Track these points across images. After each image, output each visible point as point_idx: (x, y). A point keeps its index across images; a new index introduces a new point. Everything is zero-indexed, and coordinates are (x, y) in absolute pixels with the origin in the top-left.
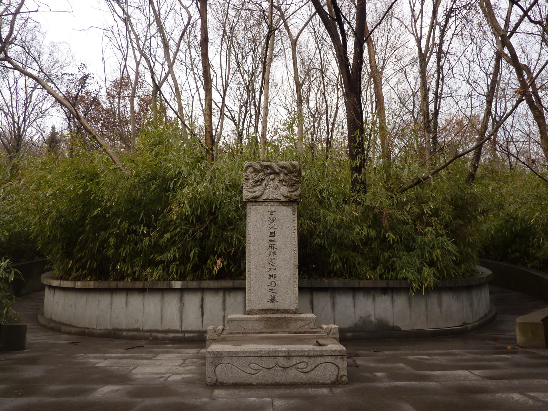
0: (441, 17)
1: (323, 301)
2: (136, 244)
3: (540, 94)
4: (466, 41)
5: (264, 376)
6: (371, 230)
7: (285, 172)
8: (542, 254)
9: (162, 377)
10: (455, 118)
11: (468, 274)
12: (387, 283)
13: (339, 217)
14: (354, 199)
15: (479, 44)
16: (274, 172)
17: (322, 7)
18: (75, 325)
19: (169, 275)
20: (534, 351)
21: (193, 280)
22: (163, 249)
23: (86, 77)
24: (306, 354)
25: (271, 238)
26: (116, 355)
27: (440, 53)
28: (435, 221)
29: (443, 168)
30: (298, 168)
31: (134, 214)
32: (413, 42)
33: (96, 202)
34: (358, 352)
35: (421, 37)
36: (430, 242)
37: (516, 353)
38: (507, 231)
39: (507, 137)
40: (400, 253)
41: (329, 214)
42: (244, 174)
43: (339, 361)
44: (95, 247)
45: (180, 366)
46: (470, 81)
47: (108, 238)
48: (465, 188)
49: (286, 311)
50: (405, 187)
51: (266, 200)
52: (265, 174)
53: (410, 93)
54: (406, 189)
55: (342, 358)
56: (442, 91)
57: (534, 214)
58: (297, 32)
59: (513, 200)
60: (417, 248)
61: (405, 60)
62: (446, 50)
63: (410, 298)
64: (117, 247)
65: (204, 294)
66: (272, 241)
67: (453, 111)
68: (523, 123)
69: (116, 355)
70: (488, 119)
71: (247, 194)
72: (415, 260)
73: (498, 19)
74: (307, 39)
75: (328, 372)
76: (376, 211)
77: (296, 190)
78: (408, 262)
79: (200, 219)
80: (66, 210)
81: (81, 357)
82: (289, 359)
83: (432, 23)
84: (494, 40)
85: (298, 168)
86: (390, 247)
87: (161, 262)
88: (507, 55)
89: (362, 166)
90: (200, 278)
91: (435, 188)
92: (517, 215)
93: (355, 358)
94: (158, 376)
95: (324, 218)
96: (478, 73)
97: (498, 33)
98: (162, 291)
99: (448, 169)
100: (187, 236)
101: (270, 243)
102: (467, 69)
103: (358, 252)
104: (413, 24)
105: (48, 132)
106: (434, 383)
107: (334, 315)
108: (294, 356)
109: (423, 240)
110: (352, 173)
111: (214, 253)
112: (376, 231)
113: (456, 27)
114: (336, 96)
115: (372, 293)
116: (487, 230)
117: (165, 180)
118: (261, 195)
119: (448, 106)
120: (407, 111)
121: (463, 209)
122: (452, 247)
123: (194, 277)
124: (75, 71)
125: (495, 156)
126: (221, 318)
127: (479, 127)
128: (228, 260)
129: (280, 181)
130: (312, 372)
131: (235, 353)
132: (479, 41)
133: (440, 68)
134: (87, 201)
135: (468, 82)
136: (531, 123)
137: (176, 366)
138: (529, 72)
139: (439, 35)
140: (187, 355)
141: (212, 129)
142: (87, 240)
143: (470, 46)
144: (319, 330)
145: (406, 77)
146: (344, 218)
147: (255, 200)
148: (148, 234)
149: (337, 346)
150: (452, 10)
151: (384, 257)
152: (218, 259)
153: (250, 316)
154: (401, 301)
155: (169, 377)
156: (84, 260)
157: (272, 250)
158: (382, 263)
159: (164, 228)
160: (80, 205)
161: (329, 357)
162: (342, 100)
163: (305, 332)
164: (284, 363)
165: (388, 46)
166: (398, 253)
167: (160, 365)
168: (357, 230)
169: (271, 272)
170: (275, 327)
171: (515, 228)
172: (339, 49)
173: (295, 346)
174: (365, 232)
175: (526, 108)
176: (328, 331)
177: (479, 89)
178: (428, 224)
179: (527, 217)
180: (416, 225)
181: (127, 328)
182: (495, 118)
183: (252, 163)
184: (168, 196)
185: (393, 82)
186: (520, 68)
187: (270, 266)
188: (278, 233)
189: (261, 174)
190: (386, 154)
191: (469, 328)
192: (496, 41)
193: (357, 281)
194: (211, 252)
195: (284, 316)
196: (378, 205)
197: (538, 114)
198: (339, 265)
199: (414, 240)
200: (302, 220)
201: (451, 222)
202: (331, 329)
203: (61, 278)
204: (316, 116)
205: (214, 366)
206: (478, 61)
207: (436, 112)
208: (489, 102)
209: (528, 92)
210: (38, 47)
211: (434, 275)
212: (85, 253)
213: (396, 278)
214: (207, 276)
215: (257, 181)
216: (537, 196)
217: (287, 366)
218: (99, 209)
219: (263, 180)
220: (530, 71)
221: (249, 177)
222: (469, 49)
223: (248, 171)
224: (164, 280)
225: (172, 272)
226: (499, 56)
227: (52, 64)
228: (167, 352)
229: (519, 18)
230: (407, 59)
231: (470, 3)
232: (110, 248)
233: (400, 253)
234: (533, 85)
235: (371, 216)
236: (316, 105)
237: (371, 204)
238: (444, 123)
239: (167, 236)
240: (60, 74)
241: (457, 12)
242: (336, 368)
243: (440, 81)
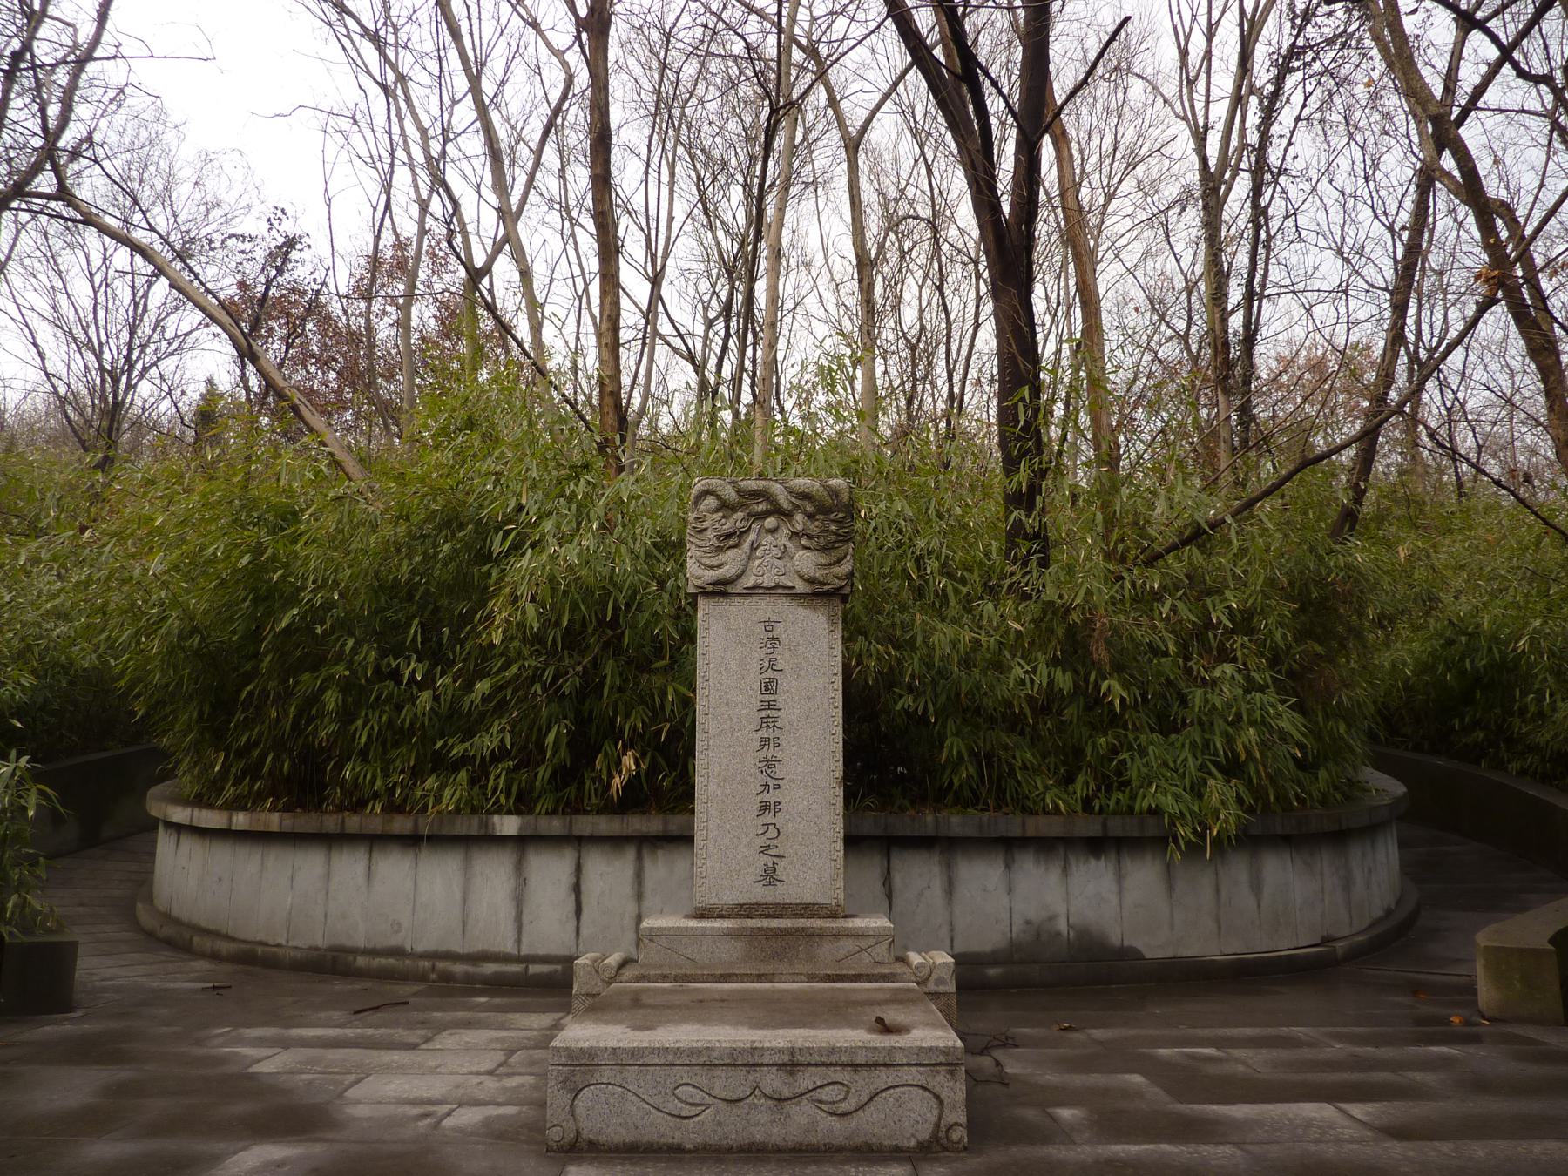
0: (1262, 73)
1: (919, 876)
2: (399, 708)
3: (1546, 286)
4: (1334, 141)
5: (719, 1124)
6: (1059, 671)
7: (809, 508)
8: (1548, 736)
9: (425, 1116)
10: (1304, 353)
11: (1338, 796)
12: (1104, 825)
13: (967, 636)
14: (1010, 586)
15: (1371, 148)
16: (777, 511)
17: (929, 50)
18: (231, 933)
19: (485, 794)
20: (1530, 1032)
21: (552, 812)
22: (471, 726)
23: (291, 243)
24: (844, 1059)
25: (767, 698)
26: (319, 1032)
27: (1262, 174)
28: (1243, 645)
29: (1267, 493)
30: (845, 497)
31: (388, 627)
32: (1184, 143)
33: (288, 590)
34: (1014, 1030)
35: (1206, 128)
36: (1229, 706)
37: (1475, 1039)
38: (1449, 669)
39: (1449, 404)
40: (1143, 738)
41: (940, 626)
42: (691, 517)
43: (940, 1081)
44: (287, 715)
45: (491, 1073)
46: (1346, 250)
47: (322, 690)
48: (1330, 552)
49: (808, 910)
50: (1158, 548)
51: (753, 591)
53: (1180, 284)
54: (1160, 556)
55: (951, 1073)
56: (1265, 276)
57: (1527, 624)
58: (864, 114)
59: (1467, 581)
60: (1192, 723)
61: (1166, 193)
62: (1278, 164)
63: (1168, 868)
64: (346, 716)
66: (769, 706)
67: (1299, 332)
68: (1494, 366)
69: (319, 1032)
70: (1396, 356)
71: (697, 569)
72: (1186, 759)
73: (1426, 72)
74: (894, 136)
75: (909, 1114)
76: (1075, 617)
77: (838, 561)
78: (1165, 764)
79: (574, 639)
80: (205, 613)
81: (221, 1040)
82: (792, 1073)
83: (1238, 88)
84: (1415, 139)
85: (845, 497)
86: (1115, 720)
87: (464, 760)
88: (1448, 174)
89: (1034, 489)
90: (574, 808)
91: (1243, 551)
92: (1478, 626)
93: (999, 1054)
94: (416, 1111)
96: (1369, 228)
97: (1424, 110)
98: (468, 842)
99: (1283, 497)
100: (538, 688)
101: (764, 714)
102: (1337, 218)
103: (1022, 733)
104: (1185, 90)
105: (195, 392)
106: (1228, 1150)
108: (809, 1065)
109: (1207, 701)
110: (1007, 508)
111: (615, 735)
112: (1076, 672)
113: (1306, 98)
114: (973, 294)
115: (1062, 852)
116: (1393, 665)
117: (484, 530)
118: (739, 576)
119: (1286, 320)
120: (1169, 332)
121: (1323, 612)
122: (1289, 722)
123: (557, 802)
124: (251, 225)
125: (1416, 458)
127: (1370, 376)
128: (653, 757)
129: (795, 535)
130: (860, 1113)
131: (635, 1052)
132: (1371, 139)
133: (1259, 215)
134: (264, 590)
135: (1340, 252)
136: (1515, 365)
137: (478, 1073)
138: (1512, 223)
139: (1258, 121)
140: (522, 1034)
141: (620, 388)
142: (265, 693)
143: (1346, 151)
144: (899, 968)
145: (1167, 237)
146: (983, 639)
147: (720, 590)
148: (428, 681)
149: (939, 1033)
150: (1294, 52)
151: (1094, 744)
152: (624, 753)
153: (704, 924)
154: (1144, 875)
155: (449, 1114)
156: (256, 753)
157: (771, 734)
158: (1090, 766)
159: (477, 665)
160: (244, 600)
161: (914, 1069)
162: (988, 308)
163: (856, 978)
164: (777, 1084)
165: (1118, 155)
166: (1136, 739)
167: (433, 1071)
168: (1018, 672)
169: (766, 797)
170: (775, 955)
171: (1472, 662)
172: (972, 161)
173: (812, 1032)
174: (1041, 678)
175: (1502, 324)
176: (924, 973)
177: (1370, 272)
178: (1225, 656)
179: (1507, 631)
180: (1187, 658)
181: (370, 945)
182: (1416, 352)
184: (489, 575)
185: (1131, 256)
186: (1486, 210)
187: (764, 779)
188: (786, 683)
189: (740, 515)
190: (1109, 458)
191: (1340, 952)
192: (1420, 134)
193: (1018, 819)
194: (597, 735)
196: (1078, 600)
197: (1539, 341)
198: (966, 771)
199: (1184, 701)
200: (860, 644)
201: (1289, 647)
202: (933, 968)
203: (199, 801)
204: (918, 350)
205: (570, 1091)
206: (1366, 195)
207: (1250, 339)
208: (1400, 309)
209: (1510, 279)
210: (164, 165)
211: (1240, 800)
212: (260, 734)
213: (1131, 810)
214: (594, 801)
215: (729, 536)
216: (1534, 573)
217: (787, 1094)
218: (295, 612)
219: (744, 533)
220: (1515, 220)
221: (705, 525)
222: (1343, 163)
223: (702, 507)
224: (474, 811)
225: (495, 790)
226: (1426, 179)
227: (203, 208)
228: (468, 1025)
229: (1484, 69)
230: (1171, 191)
231: (1345, 31)
232: (326, 720)
233: (1143, 738)
234: (1525, 257)
235: (1060, 632)
236: (920, 319)
237: (1061, 597)
238: (1274, 365)
239: (483, 687)
240: (217, 238)
241: (1309, 56)
242: (934, 1102)
243: (1261, 250)
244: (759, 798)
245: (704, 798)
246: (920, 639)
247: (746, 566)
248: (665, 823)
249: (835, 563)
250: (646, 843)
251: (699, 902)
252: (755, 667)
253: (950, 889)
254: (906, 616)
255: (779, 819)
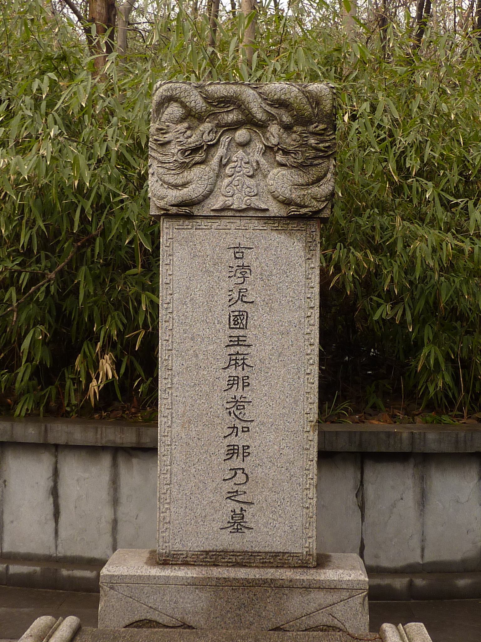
1: (392, 488)
7: (286, 118)
16: (250, 121)
25: (236, 332)
30: (327, 105)
49: (278, 559)
51: (222, 213)
52: (218, 126)
65: (60, 457)
66: (238, 341)
71: (161, 190)
77: (318, 181)
85: (327, 105)
90: (55, 412)
95: (406, 245)
100: (12, 291)
101: (232, 350)
107: (423, 525)
118: (206, 197)
126: (106, 527)
129: (269, 149)
147: (186, 211)
153: (168, 572)
157: (240, 372)
169: (233, 440)
183: (178, 86)
187: (231, 420)
188: (258, 317)
189: (207, 126)
195: (270, 573)
198: (443, 380)
200: (338, 253)
215: (195, 150)
221: (168, 137)
223: (165, 117)
244: (227, 442)
245: (168, 440)
246: (400, 246)
247: (214, 184)
248: (139, 435)
249: (313, 183)
250: (118, 452)
251: (162, 548)
252: (222, 298)
253: (423, 500)
254: (385, 220)
255: (248, 464)
